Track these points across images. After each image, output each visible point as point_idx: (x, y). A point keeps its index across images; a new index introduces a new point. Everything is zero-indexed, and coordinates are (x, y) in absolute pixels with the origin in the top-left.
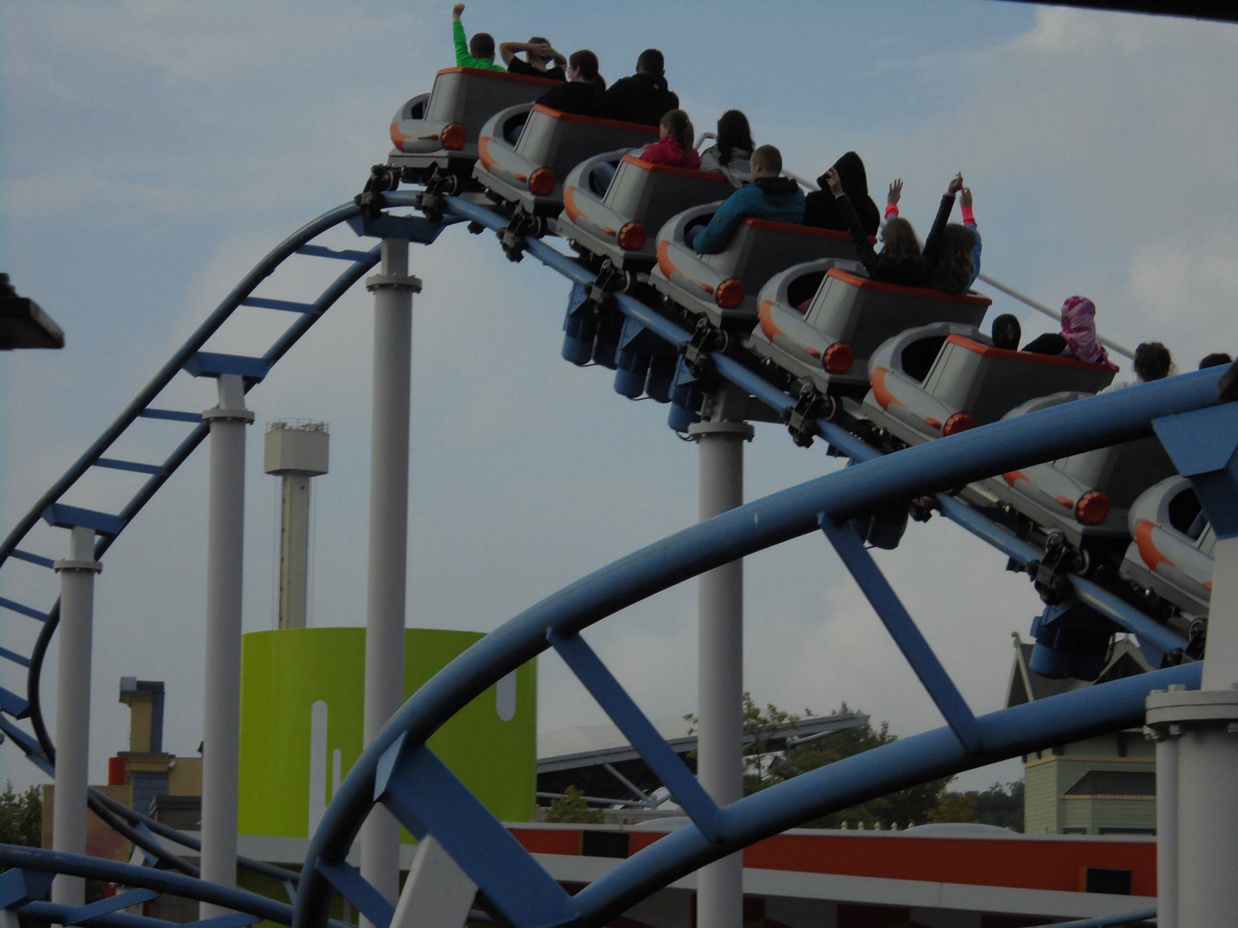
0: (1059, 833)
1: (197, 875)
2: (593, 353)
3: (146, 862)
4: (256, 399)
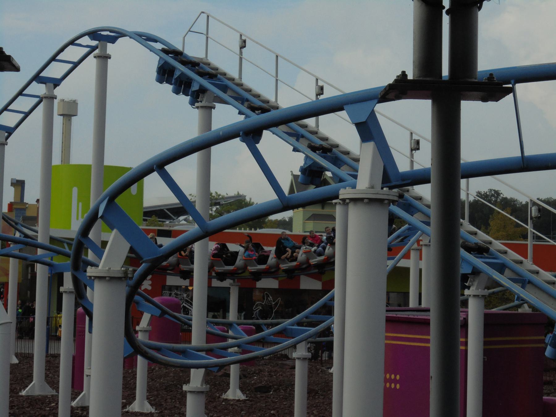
0: (303, 232)
1: (37, 240)
2: (165, 79)
3: (20, 236)
4: (57, 91)
